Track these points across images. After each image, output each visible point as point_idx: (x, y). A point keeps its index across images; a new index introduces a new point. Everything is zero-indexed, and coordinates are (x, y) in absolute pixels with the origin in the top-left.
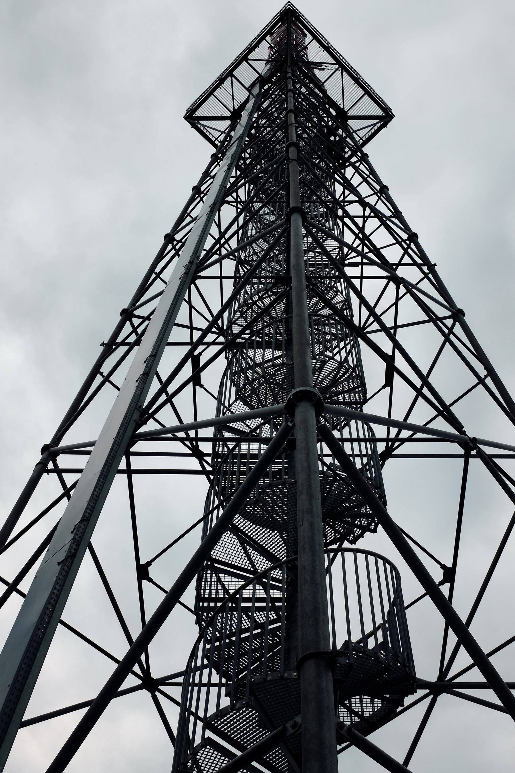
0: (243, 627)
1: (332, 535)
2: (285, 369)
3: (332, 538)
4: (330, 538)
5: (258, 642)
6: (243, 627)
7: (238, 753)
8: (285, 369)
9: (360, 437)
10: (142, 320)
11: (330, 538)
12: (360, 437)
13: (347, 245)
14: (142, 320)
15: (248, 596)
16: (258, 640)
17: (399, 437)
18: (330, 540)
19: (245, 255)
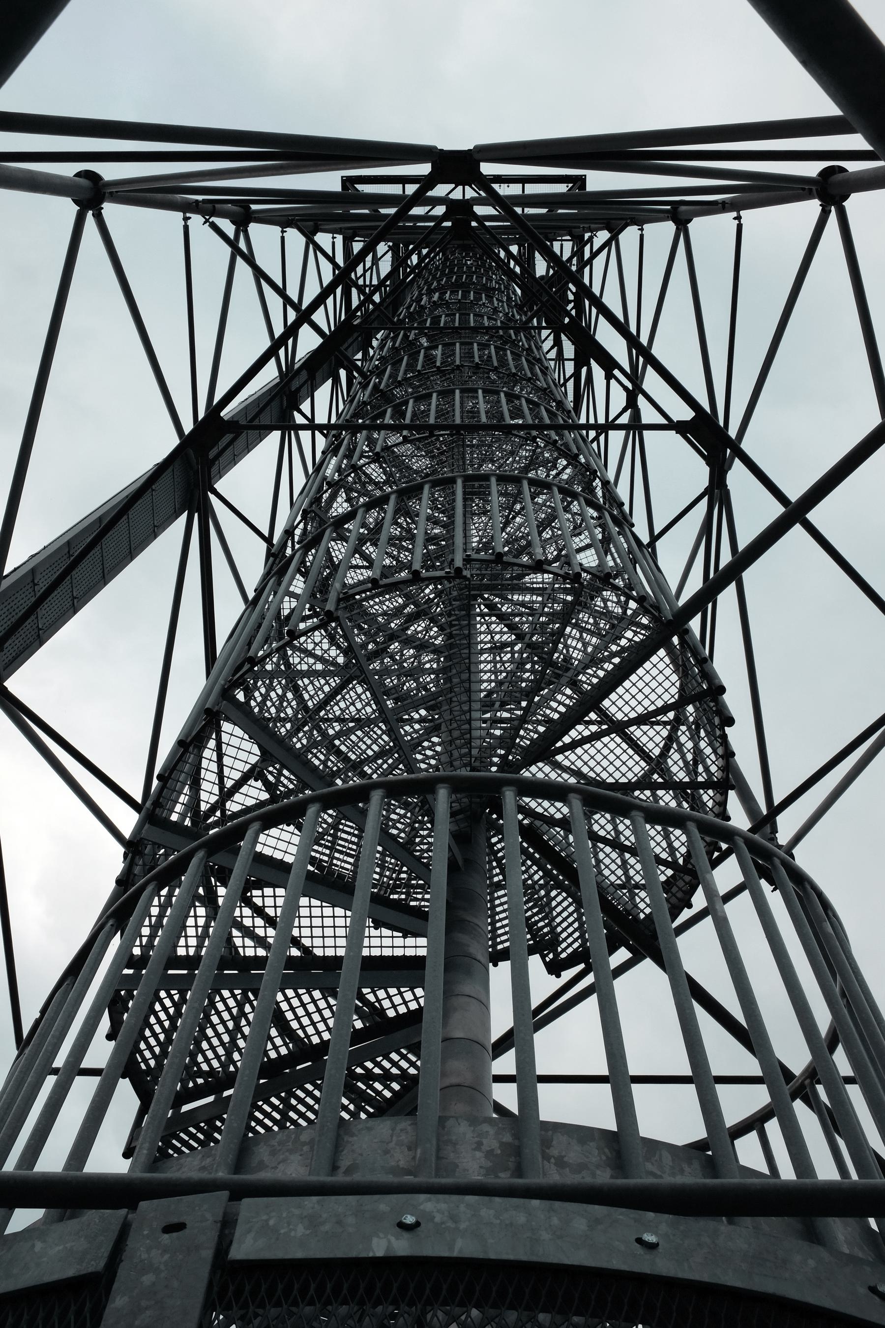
0: (273, 1055)
1: (571, 919)
2: (439, 744)
3: (576, 945)
4: (570, 945)
5: (274, 1108)
6: (273, 1055)
7: (854, 1176)
8: (439, 744)
9: (599, 422)
10: (267, 535)
11: (570, 945)
12: (599, 422)
13: (526, 1060)
14: (267, 535)
15: (278, 855)
16: (274, 1100)
17: (740, 550)
18: (570, 950)
19: (372, 481)
